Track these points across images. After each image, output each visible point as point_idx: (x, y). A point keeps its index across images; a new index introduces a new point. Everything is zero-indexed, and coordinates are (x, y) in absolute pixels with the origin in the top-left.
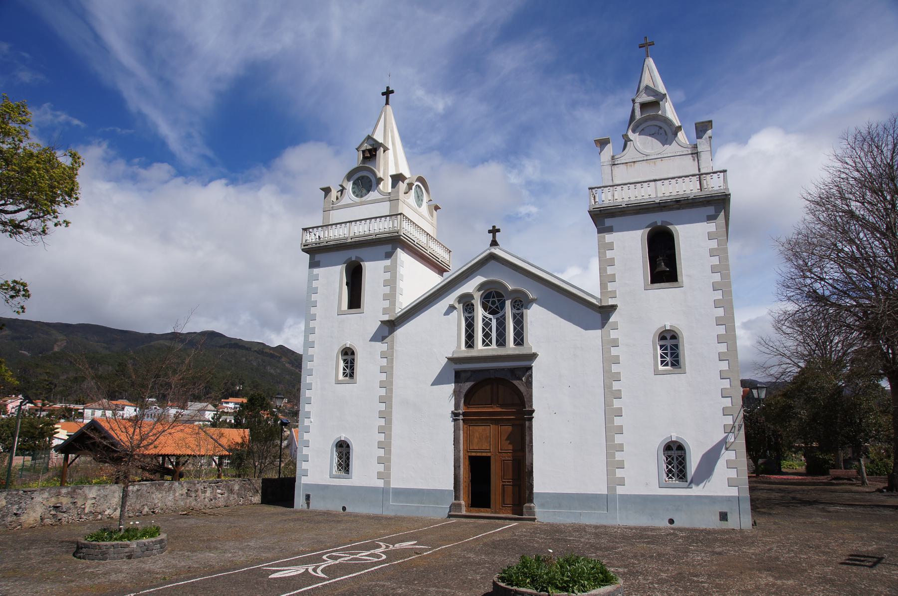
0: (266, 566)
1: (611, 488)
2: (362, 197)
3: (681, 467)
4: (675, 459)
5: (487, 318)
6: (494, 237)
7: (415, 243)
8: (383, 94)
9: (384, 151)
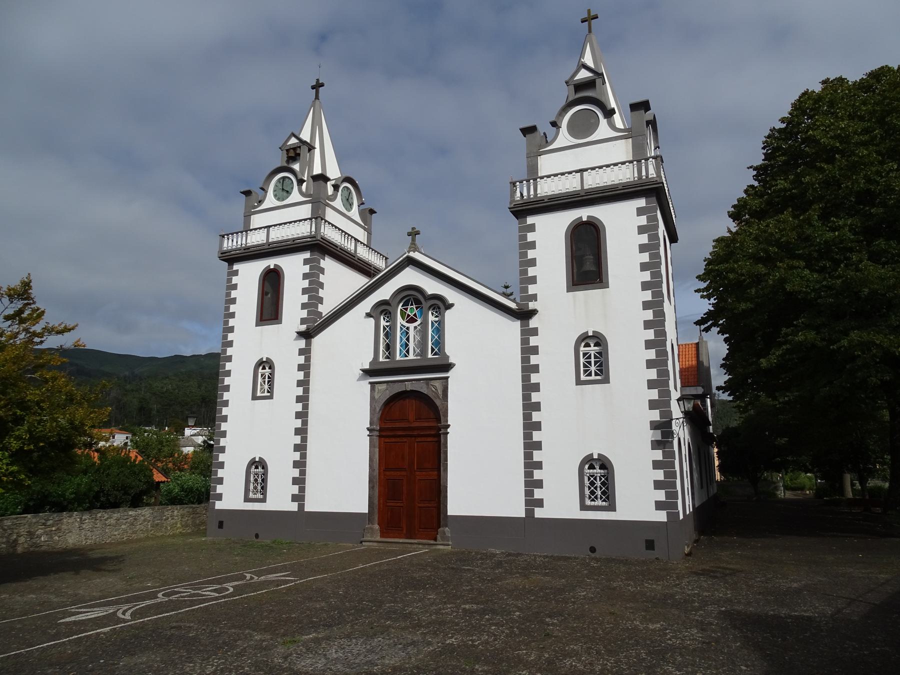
1: (530, 513)
2: (283, 200)
3: (592, 488)
5: (404, 327)
6: (413, 240)
7: (338, 249)
8: (313, 87)
9: (310, 150)
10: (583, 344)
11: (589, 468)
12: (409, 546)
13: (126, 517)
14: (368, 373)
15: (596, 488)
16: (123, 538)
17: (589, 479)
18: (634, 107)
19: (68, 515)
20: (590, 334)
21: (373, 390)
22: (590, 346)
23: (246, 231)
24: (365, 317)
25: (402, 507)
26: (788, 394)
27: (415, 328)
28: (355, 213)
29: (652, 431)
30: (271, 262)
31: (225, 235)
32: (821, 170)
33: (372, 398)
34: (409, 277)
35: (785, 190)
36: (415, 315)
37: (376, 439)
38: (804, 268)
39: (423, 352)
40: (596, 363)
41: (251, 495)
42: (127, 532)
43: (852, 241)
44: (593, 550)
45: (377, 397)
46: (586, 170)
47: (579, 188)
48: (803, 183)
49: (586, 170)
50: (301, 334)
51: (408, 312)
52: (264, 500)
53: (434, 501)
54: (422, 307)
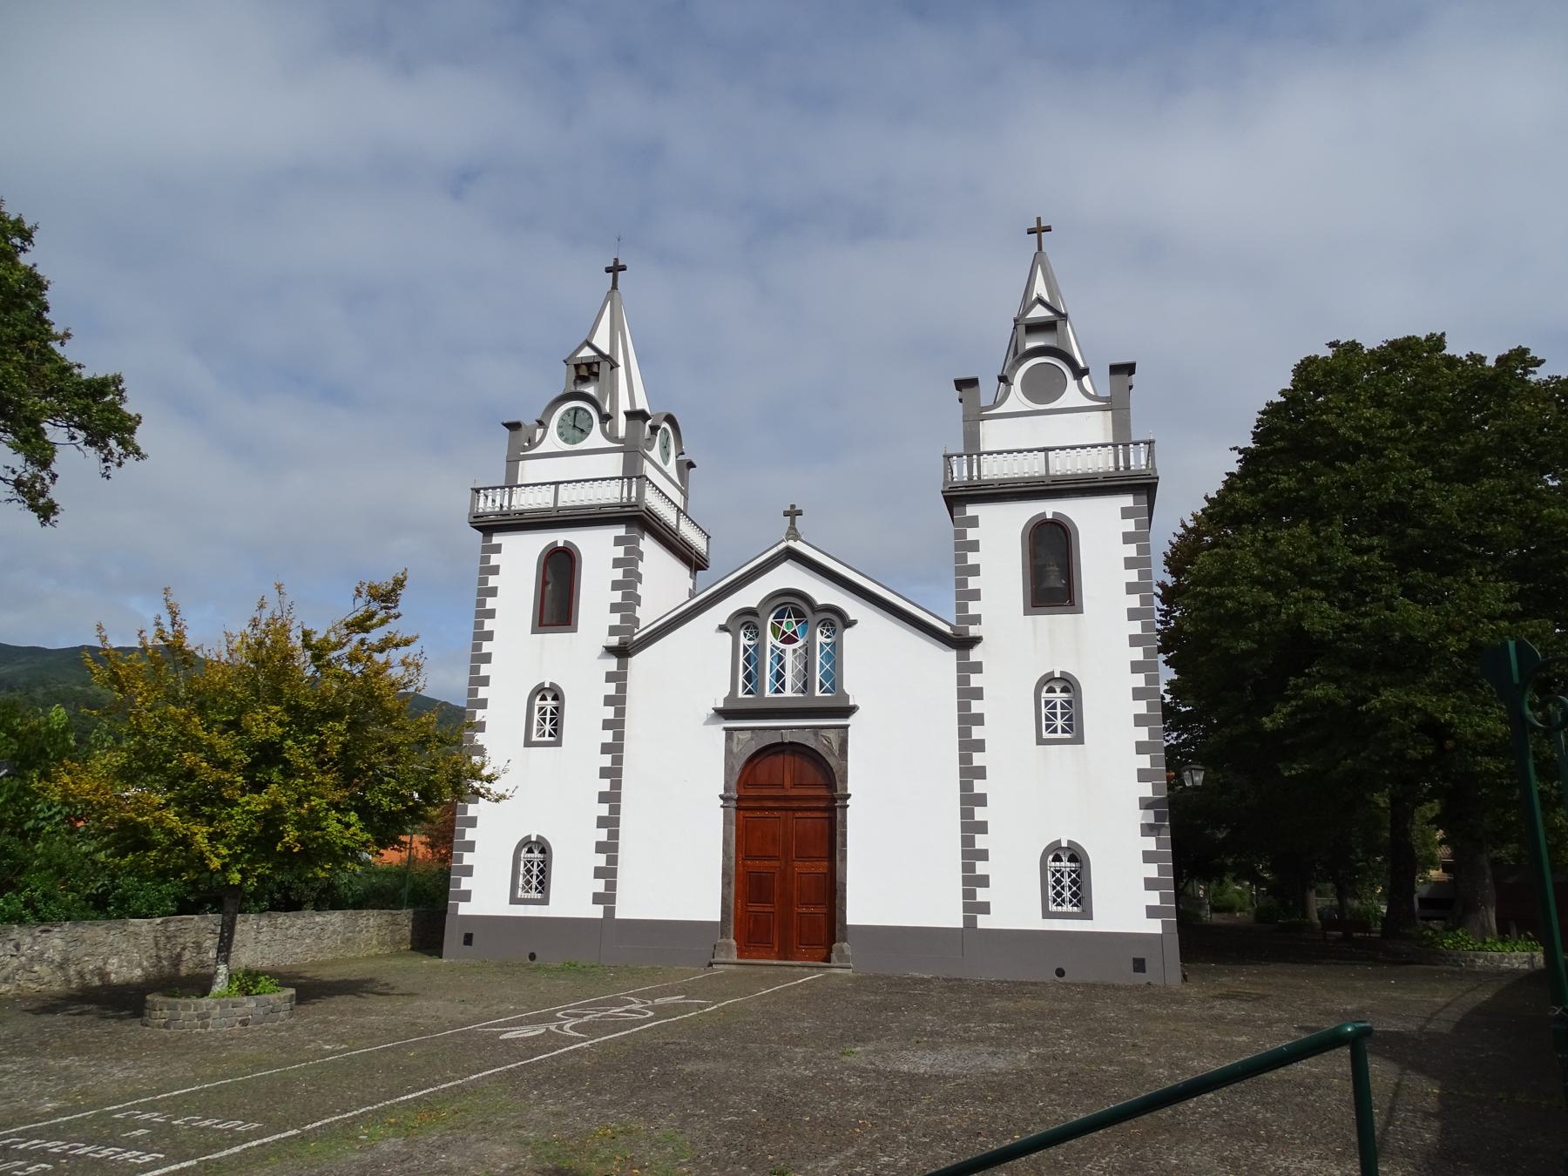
0: (486, 1027)
1: (970, 922)
2: (574, 443)
4: (1066, 875)
5: (778, 648)
6: (793, 522)
7: (662, 524)
8: (608, 270)
9: (612, 368)
10: (1045, 688)
11: (1054, 860)
12: (787, 969)
13: (312, 926)
14: (723, 714)
15: (1063, 888)
16: (307, 959)
17: (1054, 875)
18: (1116, 369)
19: (242, 919)
20: (1057, 675)
21: (729, 738)
22: (1055, 692)
23: (511, 487)
24: (716, 631)
25: (773, 913)
26: (1295, 766)
27: (795, 651)
28: (671, 468)
29: (1142, 811)
30: (560, 537)
31: (482, 489)
32: (1342, 471)
33: (729, 752)
34: (788, 577)
35: (1290, 490)
36: (794, 632)
37: (733, 811)
38: (1322, 599)
39: (806, 686)
40: (1063, 715)
41: (520, 894)
42: (311, 950)
43: (1382, 569)
44: (1060, 973)
45: (735, 750)
46: (1053, 449)
47: (1043, 472)
48: (1315, 485)
49: (1053, 449)
50: (610, 651)
51: (784, 627)
52: (545, 901)
53: (822, 904)
54: (806, 622)
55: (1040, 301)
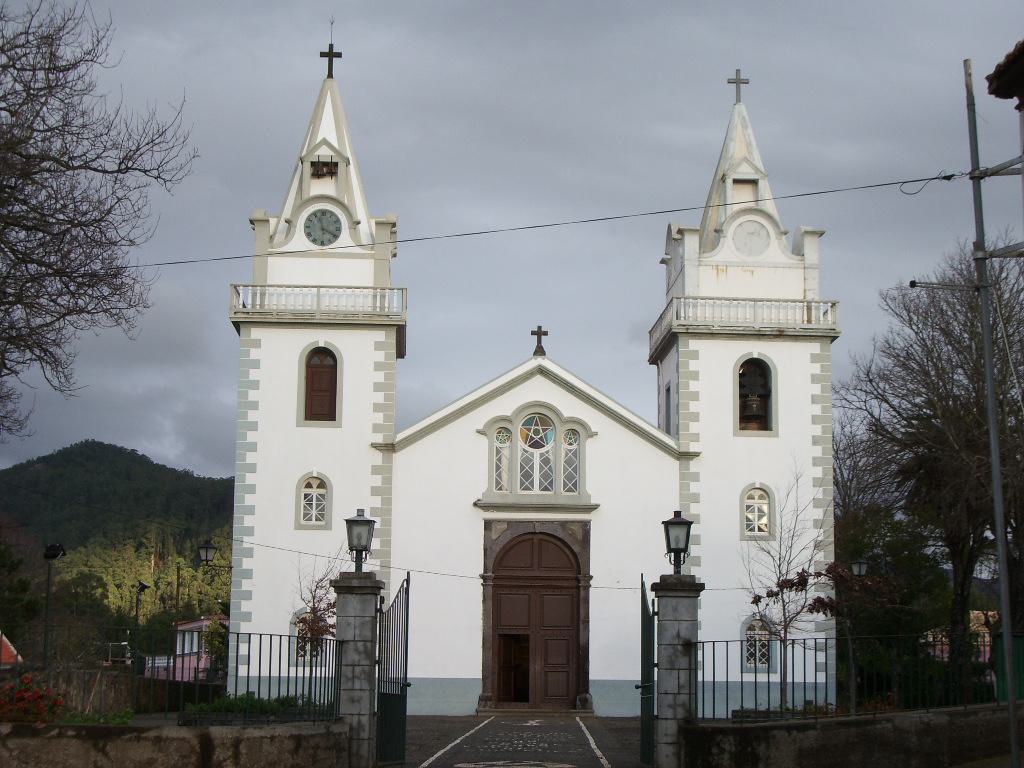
5: (526, 452)
6: (539, 341)
20: (315, 475)
22: (754, 499)
55: (325, 142)
